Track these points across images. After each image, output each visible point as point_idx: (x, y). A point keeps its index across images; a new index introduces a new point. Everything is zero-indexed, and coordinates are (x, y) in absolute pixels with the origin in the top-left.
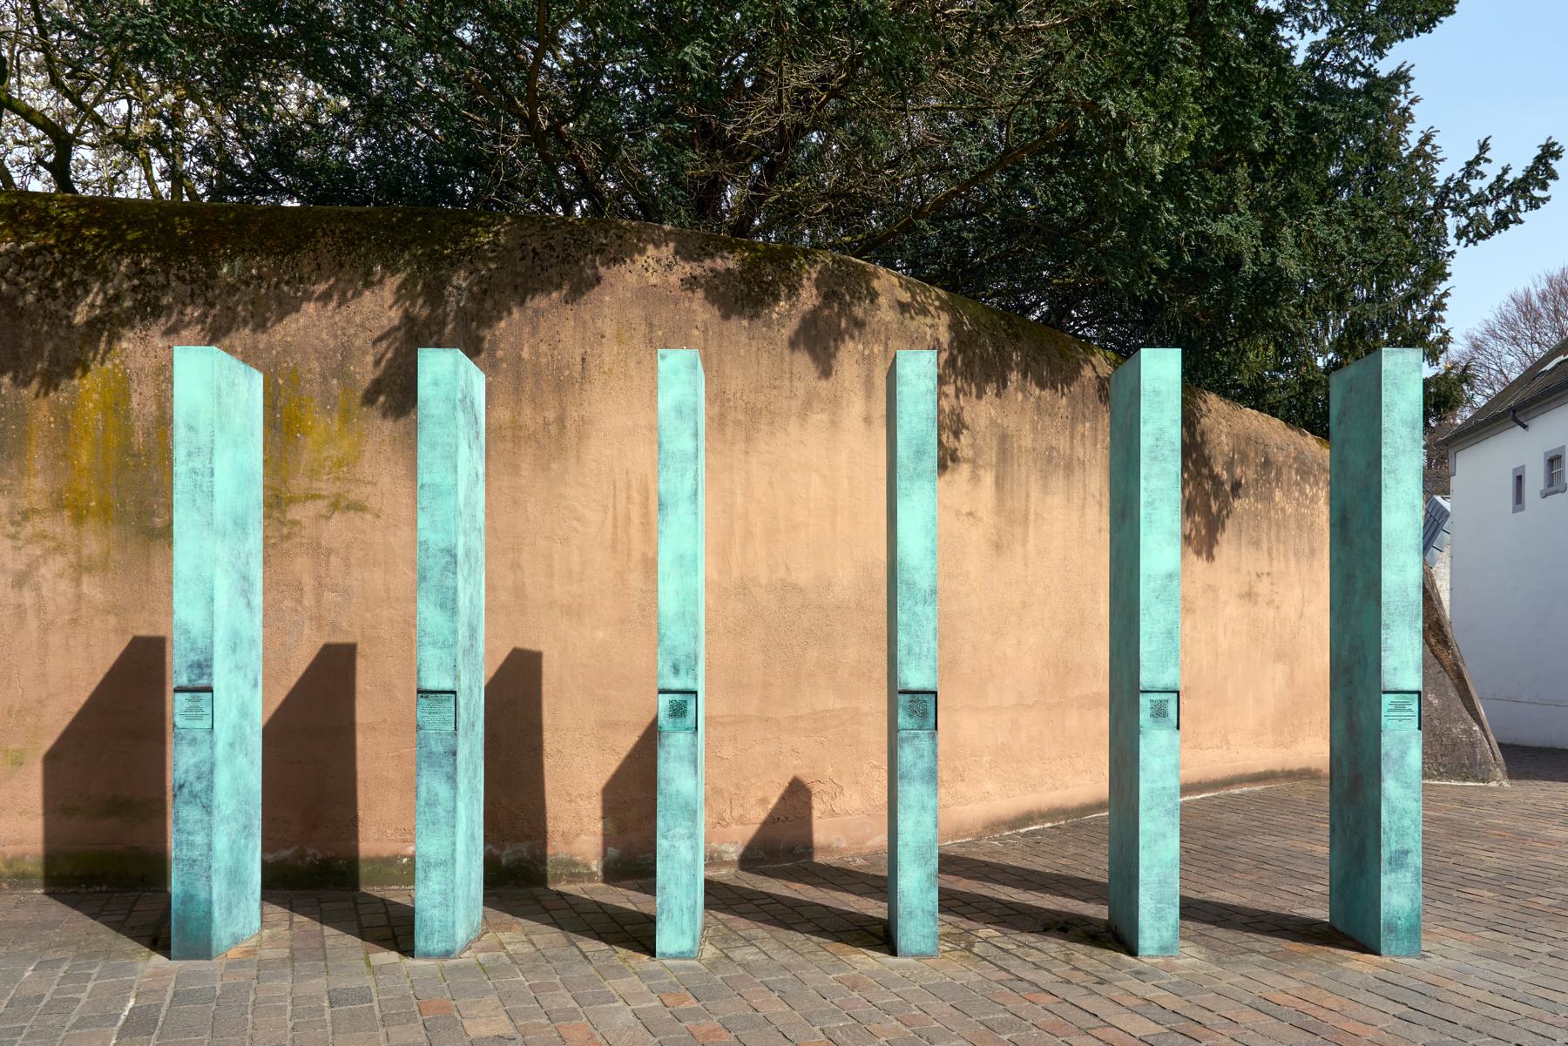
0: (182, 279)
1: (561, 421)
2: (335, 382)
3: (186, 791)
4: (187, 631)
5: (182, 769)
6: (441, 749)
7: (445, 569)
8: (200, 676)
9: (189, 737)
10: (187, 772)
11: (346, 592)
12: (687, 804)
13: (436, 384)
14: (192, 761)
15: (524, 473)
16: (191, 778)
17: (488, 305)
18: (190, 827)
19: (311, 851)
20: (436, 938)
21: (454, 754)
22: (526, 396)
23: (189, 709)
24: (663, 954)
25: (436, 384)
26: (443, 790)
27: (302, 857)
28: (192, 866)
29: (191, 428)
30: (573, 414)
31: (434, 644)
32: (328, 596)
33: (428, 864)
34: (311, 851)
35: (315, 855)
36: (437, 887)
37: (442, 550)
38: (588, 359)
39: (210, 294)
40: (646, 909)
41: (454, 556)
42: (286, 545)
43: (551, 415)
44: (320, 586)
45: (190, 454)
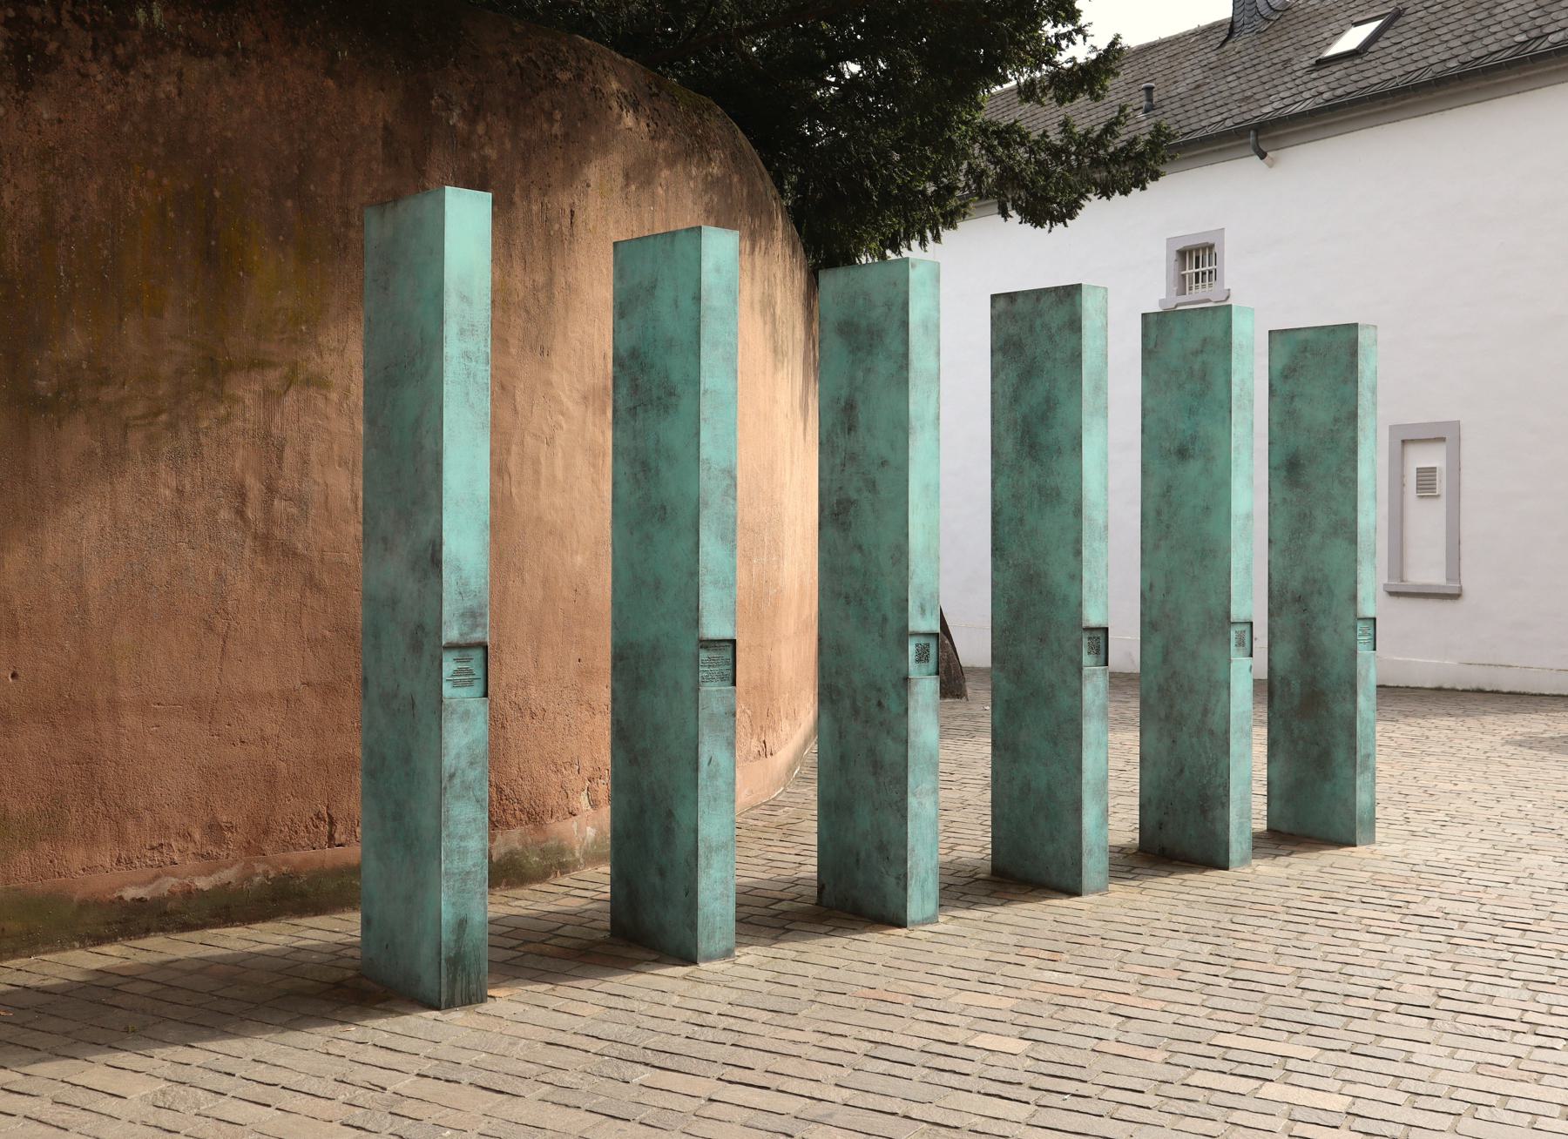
0: (79, 20)
1: (550, 283)
2: (289, 203)
3: (457, 781)
4: (459, 569)
5: (453, 753)
6: (722, 709)
7: (726, 493)
8: (474, 627)
9: (461, 710)
10: (458, 756)
11: (301, 501)
12: (932, 756)
13: (718, 270)
14: (465, 741)
15: (513, 351)
16: (463, 763)
17: (481, 129)
18: (461, 830)
19: (260, 868)
20: (718, 935)
21: (734, 715)
22: (516, 253)
23: (458, 672)
24: (913, 923)
25: (718, 270)
26: (722, 757)
27: (249, 879)
28: (464, 881)
29: (464, 298)
30: (560, 280)
31: (715, 583)
32: (278, 504)
33: (710, 849)
34: (260, 868)
35: (266, 873)
36: (718, 875)
37: (723, 471)
38: (576, 211)
39: (120, 51)
40: (1234, 855)
41: (734, 478)
42: (223, 431)
43: (540, 279)
44: (271, 490)
45: (462, 332)
